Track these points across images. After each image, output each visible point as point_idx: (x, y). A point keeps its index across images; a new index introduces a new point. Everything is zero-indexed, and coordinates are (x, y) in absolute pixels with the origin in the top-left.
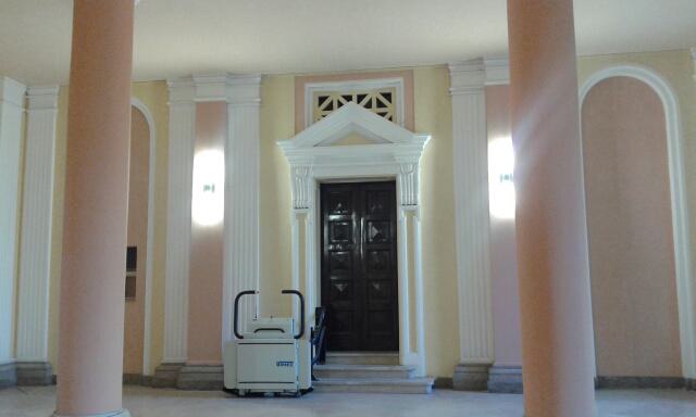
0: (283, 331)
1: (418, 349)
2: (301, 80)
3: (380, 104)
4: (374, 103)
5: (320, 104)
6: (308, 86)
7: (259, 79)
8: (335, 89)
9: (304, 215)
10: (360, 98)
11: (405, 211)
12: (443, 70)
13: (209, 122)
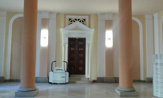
0: (62, 70)
1: (88, 74)
2: (65, 15)
3: (83, 22)
4: (81, 21)
5: (75, 19)
6: (67, 16)
7: (56, 14)
8: (73, 17)
9: (66, 45)
10: (78, 20)
11: (88, 45)
12: (96, 15)
13: (45, 23)
